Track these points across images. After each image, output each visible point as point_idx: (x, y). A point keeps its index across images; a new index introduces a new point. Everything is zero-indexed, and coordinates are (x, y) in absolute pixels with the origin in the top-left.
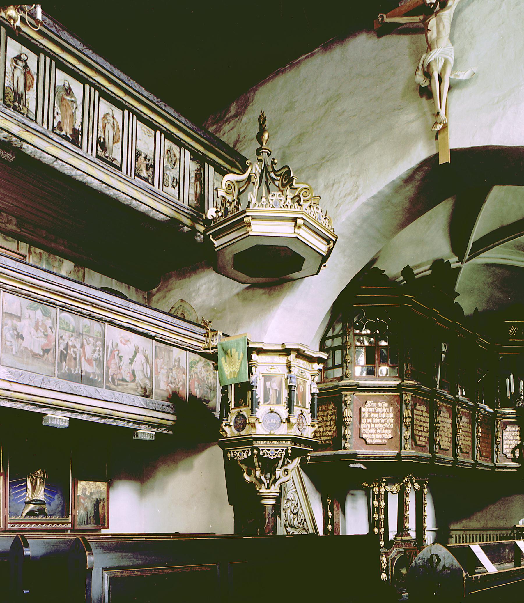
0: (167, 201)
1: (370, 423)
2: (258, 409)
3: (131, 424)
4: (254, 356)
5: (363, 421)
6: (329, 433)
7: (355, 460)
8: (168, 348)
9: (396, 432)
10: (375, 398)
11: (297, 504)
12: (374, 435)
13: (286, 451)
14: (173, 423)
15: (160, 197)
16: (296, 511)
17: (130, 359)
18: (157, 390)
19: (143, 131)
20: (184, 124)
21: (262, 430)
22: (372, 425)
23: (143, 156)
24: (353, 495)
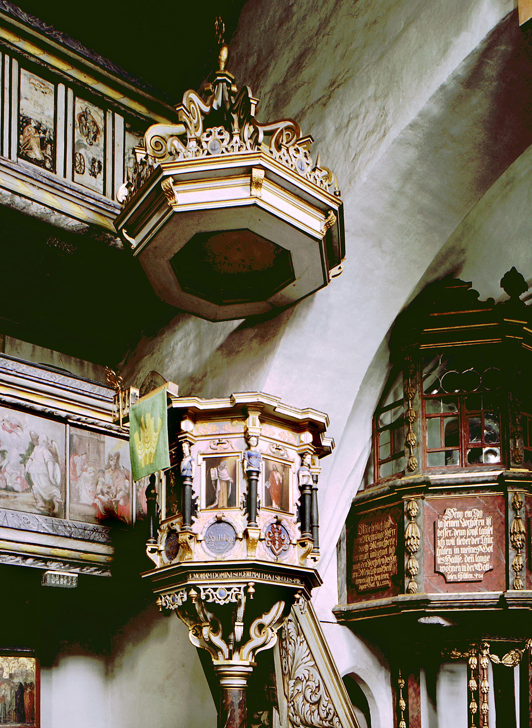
0: (80, 196)
1: (451, 547)
2: (196, 517)
3: (30, 561)
4: (186, 425)
5: (439, 543)
6: (386, 568)
7: (427, 611)
8: (96, 437)
9: (498, 560)
10: (460, 504)
11: (318, 687)
12: (459, 567)
13: (246, 589)
14: (110, 559)
15: (66, 190)
16: (315, 699)
17: (21, 455)
18: (73, 505)
19: (32, 85)
20: (102, 67)
21: (204, 554)
22: (456, 550)
23: (33, 124)
24: (452, 672)
